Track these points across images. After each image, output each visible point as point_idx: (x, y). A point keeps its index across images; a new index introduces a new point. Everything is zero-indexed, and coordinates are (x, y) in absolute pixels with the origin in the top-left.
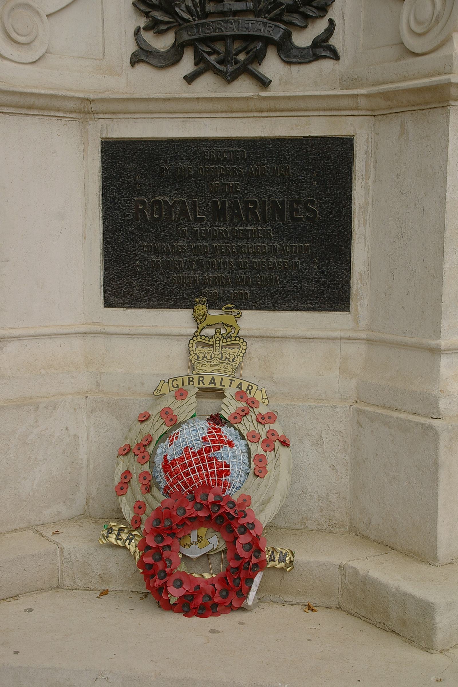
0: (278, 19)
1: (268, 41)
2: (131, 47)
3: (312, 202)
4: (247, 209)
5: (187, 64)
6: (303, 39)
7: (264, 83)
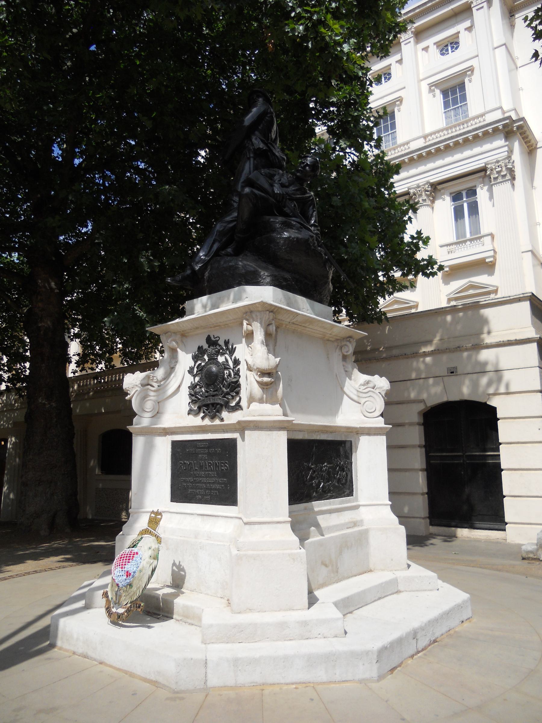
0: (224, 397)
1: (222, 406)
2: (188, 409)
3: (226, 463)
4: (209, 466)
5: (202, 414)
6: (233, 404)
7: (222, 420)
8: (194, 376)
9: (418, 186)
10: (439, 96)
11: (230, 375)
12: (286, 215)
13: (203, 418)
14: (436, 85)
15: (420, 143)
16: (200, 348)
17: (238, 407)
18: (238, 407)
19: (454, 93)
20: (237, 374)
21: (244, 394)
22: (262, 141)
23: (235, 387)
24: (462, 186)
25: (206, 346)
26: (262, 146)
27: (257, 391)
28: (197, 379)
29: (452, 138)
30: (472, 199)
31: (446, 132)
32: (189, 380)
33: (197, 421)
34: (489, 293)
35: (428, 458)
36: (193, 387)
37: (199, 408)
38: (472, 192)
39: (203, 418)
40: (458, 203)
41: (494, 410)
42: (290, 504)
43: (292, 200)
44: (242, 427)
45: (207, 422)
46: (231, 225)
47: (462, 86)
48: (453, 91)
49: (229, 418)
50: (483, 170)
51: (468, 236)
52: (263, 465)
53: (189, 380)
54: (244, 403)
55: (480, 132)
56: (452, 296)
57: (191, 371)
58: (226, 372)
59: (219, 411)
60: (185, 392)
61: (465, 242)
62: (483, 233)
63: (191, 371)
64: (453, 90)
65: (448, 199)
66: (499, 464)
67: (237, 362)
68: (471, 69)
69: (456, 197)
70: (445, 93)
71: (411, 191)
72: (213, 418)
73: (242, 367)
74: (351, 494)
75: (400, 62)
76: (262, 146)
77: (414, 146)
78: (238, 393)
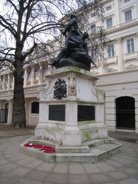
6: (64, 96)
7: (62, 100)
8: (55, 89)
9: (118, 38)
10: (124, 13)
11: (64, 89)
12: (79, 48)
13: (57, 99)
14: (123, 10)
15: (119, 26)
16: (57, 82)
17: (66, 97)
18: (66, 97)
19: (128, 13)
20: (66, 88)
21: (67, 93)
22: (74, 28)
23: (65, 92)
24: (130, 38)
25: (58, 81)
26: (74, 30)
27: (71, 93)
28: (56, 89)
29: (127, 25)
30: (132, 42)
31: (126, 24)
32: (54, 89)
33: (55, 100)
34: (115, 71)
35: (117, 111)
36: (55, 91)
37: (56, 97)
38: (132, 40)
39: (57, 99)
40: (129, 43)
41: (134, 99)
42: (78, 121)
43: (81, 44)
44: (67, 101)
45: (58, 100)
46: (65, 50)
47: (130, 11)
48: (128, 13)
49: (64, 99)
50: (135, 34)
51: (131, 52)
52: (71, 112)
53: (54, 89)
54: (67, 96)
55: (132, 25)
56: (126, 68)
57: (54, 87)
58: (63, 88)
59: (61, 98)
60: (53, 92)
61: (111, 58)
62: (135, 51)
63: (54, 87)
64: (128, 12)
65: (126, 42)
66: (135, 113)
67: (66, 85)
68: (133, 6)
69: (128, 41)
70: (126, 13)
71: (116, 39)
72: (59, 99)
73: (67, 87)
74: (94, 120)
75: (114, 4)
76: (74, 30)
77: (117, 27)
78: (66, 93)
